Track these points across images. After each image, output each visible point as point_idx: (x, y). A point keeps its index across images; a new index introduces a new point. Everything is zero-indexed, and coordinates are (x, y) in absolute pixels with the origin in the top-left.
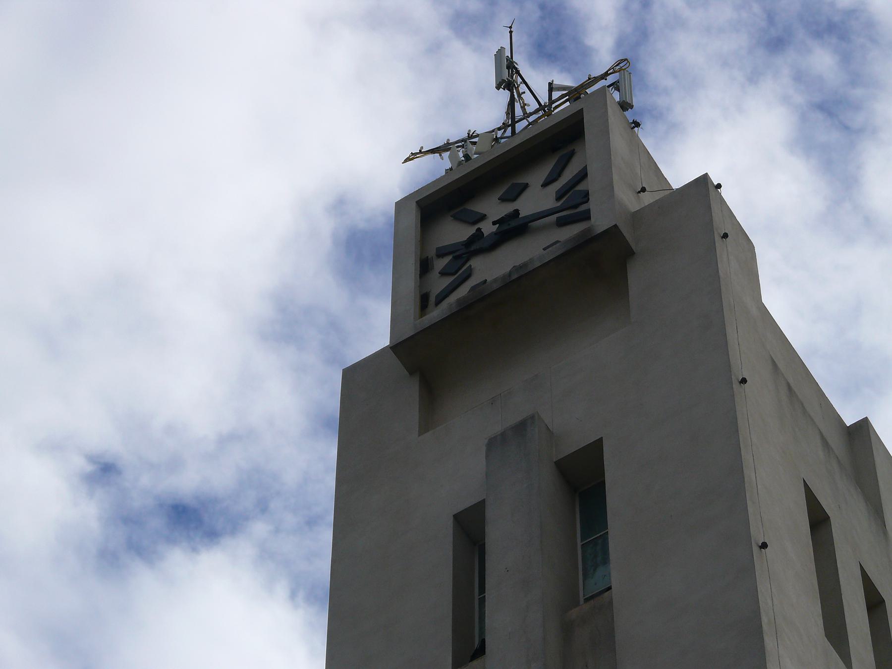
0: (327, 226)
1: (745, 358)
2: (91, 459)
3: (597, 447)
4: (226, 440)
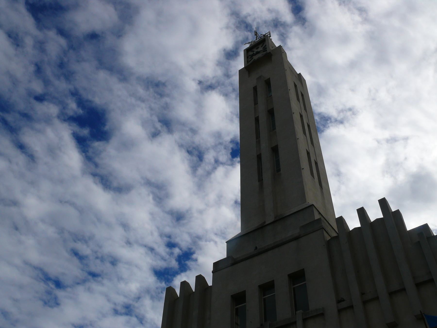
0: (223, 52)
1: (286, 67)
2: (199, 81)
3: (269, 79)
4: (214, 77)
